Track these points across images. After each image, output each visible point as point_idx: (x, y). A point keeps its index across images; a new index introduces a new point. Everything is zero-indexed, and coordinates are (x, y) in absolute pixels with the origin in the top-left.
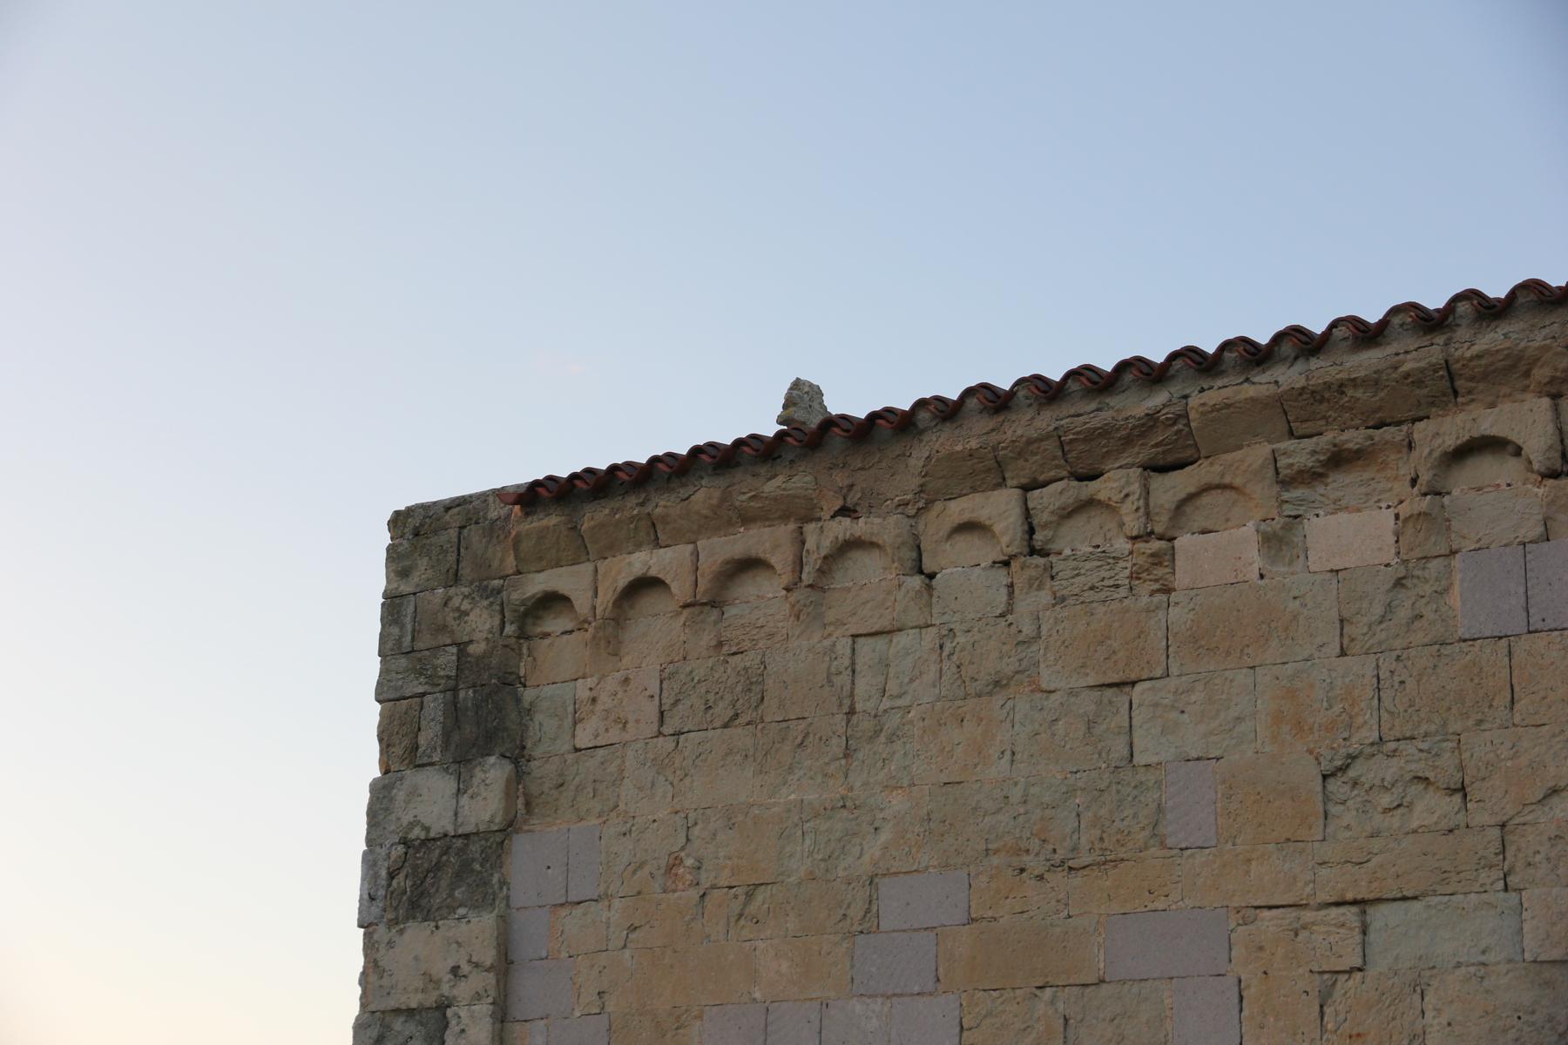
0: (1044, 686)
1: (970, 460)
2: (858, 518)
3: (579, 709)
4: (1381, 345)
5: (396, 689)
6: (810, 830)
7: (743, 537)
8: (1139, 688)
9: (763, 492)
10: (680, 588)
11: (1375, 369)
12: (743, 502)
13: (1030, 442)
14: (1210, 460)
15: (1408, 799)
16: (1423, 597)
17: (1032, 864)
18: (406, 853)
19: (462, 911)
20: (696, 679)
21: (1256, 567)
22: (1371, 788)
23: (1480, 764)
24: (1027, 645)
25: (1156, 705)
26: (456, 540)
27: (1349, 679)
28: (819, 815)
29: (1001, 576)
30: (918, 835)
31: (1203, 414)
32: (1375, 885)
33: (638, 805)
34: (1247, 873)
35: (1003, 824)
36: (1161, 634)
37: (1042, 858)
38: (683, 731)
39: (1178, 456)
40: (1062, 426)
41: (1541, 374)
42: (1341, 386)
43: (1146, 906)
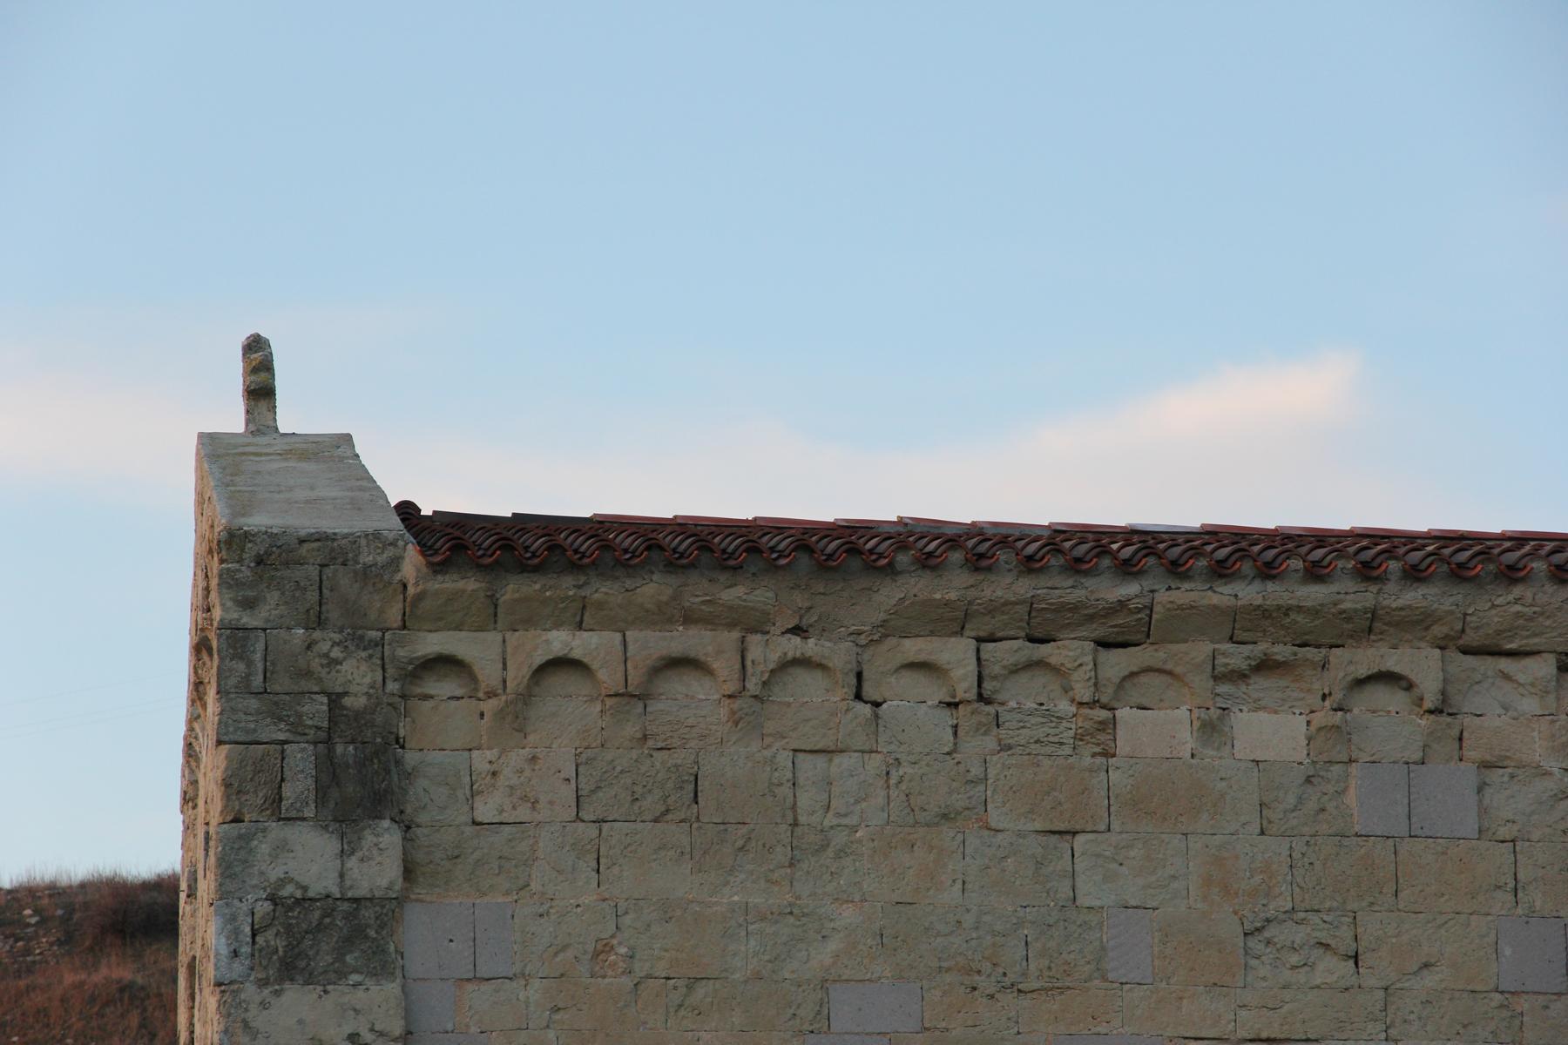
0: (993, 825)
1: (943, 608)
2: (806, 638)
3: (477, 781)
4: (1326, 582)
5: (248, 732)
6: (755, 931)
7: (681, 636)
8: (1080, 839)
9: (720, 599)
10: (609, 677)
11: (1320, 602)
12: (694, 603)
13: (1006, 603)
14: (1156, 647)
15: (1311, 960)
16: (1326, 794)
17: (984, 984)
18: (274, 910)
19: (355, 978)
20: (619, 769)
21: (1188, 747)
22: (1282, 948)
23: (1371, 938)
24: (973, 785)
25: (1098, 856)
26: (318, 579)
27: (1268, 855)
28: (766, 918)
29: (947, 718)
30: (870, 947)
31: (1169, 610)
32: (1285, 1027)
33: (559, 888)
34: (1179, 1008)
35: (955, 946)
36: (1104, 793)
37: (993, 979)
38: (606, 819)
39: (1128, 637)
40: (1039, 595)
41: (1438, 630)
42: (1288, 610)
43: (1090, 1030)
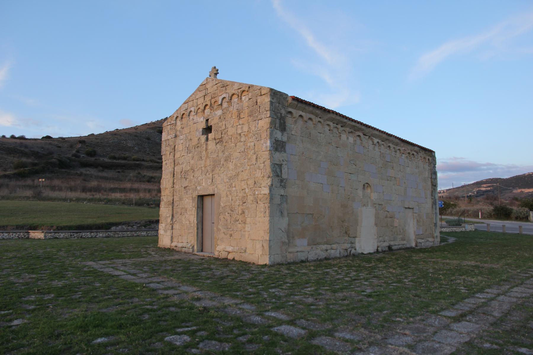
19: (283, 152)
